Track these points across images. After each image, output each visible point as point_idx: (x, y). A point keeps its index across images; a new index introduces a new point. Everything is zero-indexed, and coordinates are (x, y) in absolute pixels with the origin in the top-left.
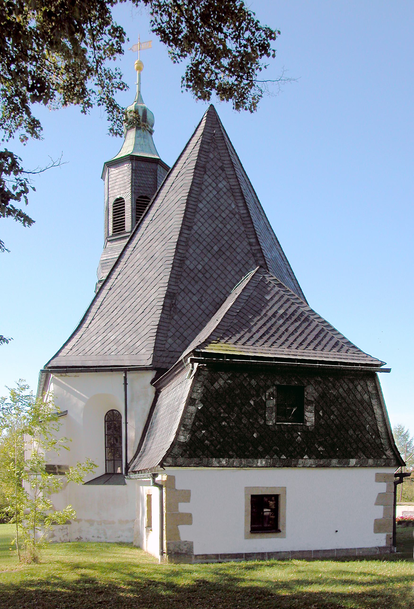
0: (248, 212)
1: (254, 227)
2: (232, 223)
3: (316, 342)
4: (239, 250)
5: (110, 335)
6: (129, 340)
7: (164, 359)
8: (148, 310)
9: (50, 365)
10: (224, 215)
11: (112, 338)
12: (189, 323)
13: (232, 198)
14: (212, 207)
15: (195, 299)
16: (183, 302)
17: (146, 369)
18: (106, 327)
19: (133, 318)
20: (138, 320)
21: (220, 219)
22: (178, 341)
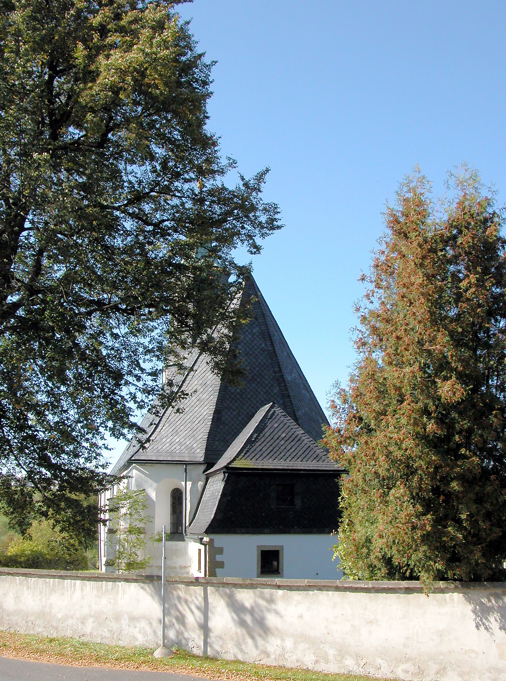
0: (274, 349)
1: (278, 359)
2: (262, 358)
3: (303, 456)
4: (266, 377)
5: (175, 438)
6: (189, 442)
7: (212, 456)
8: (202, 421)
9: (133, 458)
10: (256, 352)
11: (177, 441)
12: (230, 430)
13: (263, 340)
14: (248, 347)
15: (234, 413)
16: (227, 417)
17: (200, 464)
18: (173, 432)
19: (192, 427)
20: (195, 428)
21: (254, 355)
22: (222, 443)
